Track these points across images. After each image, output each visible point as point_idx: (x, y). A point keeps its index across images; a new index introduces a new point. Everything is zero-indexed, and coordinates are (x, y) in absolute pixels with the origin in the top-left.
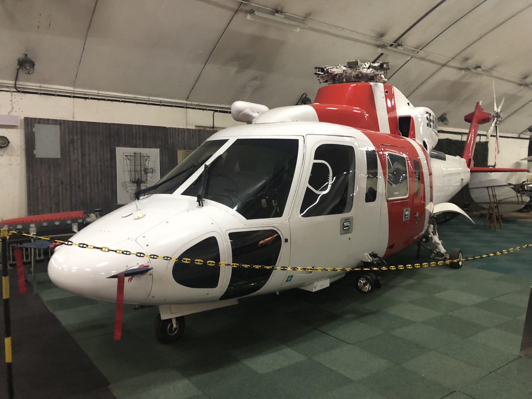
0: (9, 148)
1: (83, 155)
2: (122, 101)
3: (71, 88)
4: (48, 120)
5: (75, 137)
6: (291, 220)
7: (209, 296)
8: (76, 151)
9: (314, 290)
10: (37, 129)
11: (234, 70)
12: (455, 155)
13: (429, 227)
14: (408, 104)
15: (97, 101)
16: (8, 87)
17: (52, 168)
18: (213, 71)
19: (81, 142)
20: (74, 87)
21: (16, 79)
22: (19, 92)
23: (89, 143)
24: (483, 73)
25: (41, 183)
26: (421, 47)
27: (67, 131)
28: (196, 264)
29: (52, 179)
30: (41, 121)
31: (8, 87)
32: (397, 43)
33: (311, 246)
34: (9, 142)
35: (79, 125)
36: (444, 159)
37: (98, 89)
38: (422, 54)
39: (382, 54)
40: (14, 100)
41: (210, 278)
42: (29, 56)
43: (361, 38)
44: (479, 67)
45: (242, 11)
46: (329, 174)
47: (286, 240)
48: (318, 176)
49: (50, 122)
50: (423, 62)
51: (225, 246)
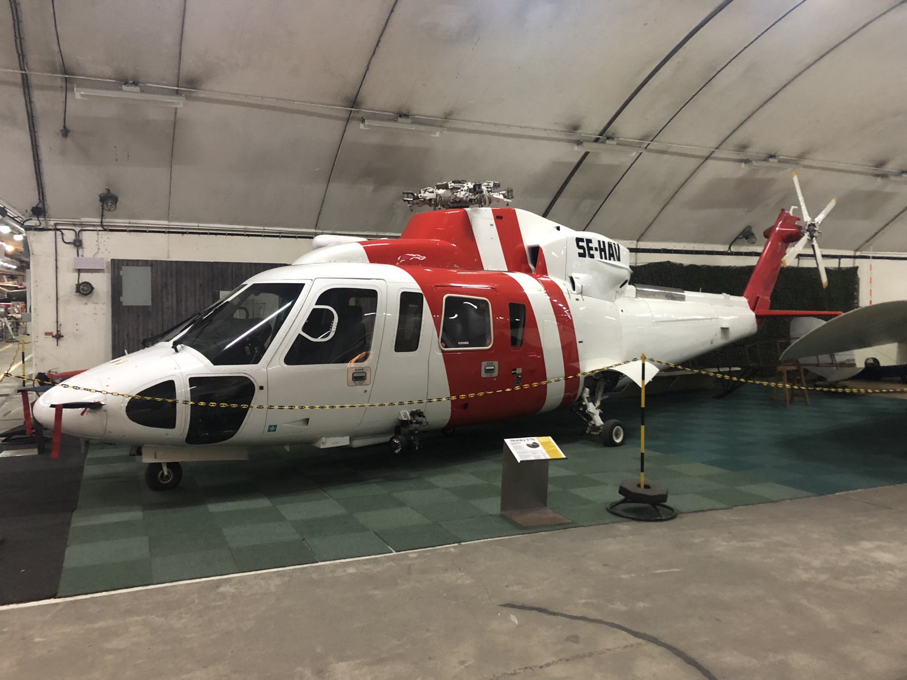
0: (94, 297)
1: (178, 302)
2: (229, 234)
3: (165, 223)
4: (138, 261)
6: (270, 367)
8: (170, 296)
9: (322, 447)
10: (125, 271)
11: (370, 188)
12: (720, 293)
13: (583, 389)
14: (558, 228)
16: (94, 226)
17: (141, 318)
18: (338, 190)
19: (177, 286)
20: (169, 220)
21: (102, 216)
22: (105, 230)
24: (781, 165)
25: (128, 336)
26: (649, 138)
28: (153, 404)
29: (141, 330)
30: (129, 263)
31: (94, 226)
32: (605, 135)
33: (286, 393)
34: (93, 288)
36: (682, 298)
37: (198, 222)
38: (654, 146)
39: (587, 154)
41: (169, 421)
42: (112, 191)
43: (544, 134)
44: (772, 156)
45: (354, 119)
47: (261, 388)
49: (140, 263)
50: (666, 157)
51: (183, 391)
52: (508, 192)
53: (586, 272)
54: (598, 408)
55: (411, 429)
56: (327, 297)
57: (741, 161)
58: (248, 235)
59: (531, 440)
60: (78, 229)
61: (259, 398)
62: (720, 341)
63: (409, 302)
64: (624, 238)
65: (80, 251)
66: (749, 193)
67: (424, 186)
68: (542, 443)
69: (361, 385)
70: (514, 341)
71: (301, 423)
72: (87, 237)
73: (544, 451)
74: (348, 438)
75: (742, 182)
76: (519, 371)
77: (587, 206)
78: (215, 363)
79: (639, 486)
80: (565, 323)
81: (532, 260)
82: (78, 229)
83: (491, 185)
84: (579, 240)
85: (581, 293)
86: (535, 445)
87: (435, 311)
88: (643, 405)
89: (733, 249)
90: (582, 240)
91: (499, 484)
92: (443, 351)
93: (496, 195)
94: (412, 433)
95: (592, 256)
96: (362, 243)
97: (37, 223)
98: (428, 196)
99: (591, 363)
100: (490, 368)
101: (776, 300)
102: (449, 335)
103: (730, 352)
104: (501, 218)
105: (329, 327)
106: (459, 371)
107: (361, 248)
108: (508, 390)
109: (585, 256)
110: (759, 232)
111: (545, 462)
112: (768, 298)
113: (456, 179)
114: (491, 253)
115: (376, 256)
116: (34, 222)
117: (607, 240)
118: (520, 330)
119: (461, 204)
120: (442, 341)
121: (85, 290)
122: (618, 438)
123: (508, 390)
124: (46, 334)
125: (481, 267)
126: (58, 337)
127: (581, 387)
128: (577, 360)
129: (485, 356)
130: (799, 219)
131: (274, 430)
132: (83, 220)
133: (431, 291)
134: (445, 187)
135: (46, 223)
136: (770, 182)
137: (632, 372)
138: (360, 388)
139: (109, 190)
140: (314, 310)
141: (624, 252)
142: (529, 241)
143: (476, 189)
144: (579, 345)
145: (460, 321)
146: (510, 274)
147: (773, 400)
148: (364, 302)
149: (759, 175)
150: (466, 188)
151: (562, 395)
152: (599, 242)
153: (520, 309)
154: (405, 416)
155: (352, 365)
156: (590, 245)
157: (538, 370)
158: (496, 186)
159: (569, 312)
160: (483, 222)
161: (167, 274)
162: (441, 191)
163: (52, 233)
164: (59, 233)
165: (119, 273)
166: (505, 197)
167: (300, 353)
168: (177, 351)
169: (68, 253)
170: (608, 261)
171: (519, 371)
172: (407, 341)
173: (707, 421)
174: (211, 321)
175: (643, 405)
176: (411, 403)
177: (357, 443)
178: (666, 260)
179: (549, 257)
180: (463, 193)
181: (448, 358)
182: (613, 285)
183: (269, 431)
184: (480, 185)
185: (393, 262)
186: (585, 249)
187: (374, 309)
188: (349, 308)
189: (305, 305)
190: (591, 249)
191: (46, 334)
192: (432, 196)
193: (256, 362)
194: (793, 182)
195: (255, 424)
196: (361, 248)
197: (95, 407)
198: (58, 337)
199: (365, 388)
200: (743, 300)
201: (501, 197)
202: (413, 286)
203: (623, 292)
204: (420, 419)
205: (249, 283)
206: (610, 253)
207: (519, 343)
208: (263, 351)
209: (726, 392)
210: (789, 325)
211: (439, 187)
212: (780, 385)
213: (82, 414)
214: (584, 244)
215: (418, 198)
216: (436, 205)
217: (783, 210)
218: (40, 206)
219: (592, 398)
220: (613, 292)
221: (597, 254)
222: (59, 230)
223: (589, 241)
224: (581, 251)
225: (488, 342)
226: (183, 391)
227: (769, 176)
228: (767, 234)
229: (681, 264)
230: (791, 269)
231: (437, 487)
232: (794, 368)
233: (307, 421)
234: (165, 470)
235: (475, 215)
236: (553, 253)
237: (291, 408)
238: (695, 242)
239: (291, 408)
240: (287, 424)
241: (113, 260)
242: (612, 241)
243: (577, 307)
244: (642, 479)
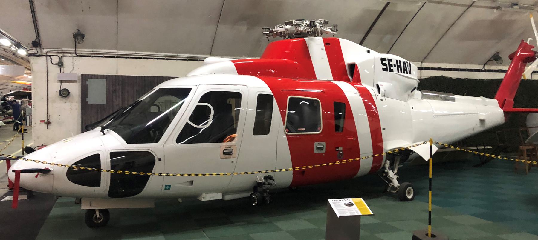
0: (70, 98)
2: (155, 59)
3: (115, 51)
5: (117, 88)
6: (166, 145)
7: (95, 192)
8: (117, 98)
9: (203, 200)
10: (90, 82)
11: (244, 28)
13: (386, 161)
14: (369, 52)
15: (135, 59)
16: (70, 53)
20: (117, 50)
21: (75, 47)
22: (78, 56)
23: (128, 92)
24: (522, 10)
27: (111, 83)
28: (85, 170)
31: (70, 53)
34: (69, 93)
35: (121, 79)
36: (454, 100)
40: (75, 62)
41: (96, 183)
42: (81, 31)
44: (515, 4)
46: (210, 113)
47: (160, 159)
48: (199, 114)
50: (441, 5)
51: (105, 162)
52: (334, 27)
53: (388, 82)
54: (396, 174)
55: (264, 188)
56: (207, 97)
57: (494, 8)
58: (168, 59)
59: (347, 201)
60: (60, 55)
61: (157, 168)
62: (479, 129)
63: (264, 101)
64: (414, 61)
65: (62, 69)
66: (498, 29)
67: (277, 24)
68: (356, 203)
69: (230, 158)
70: (337, 127)
71: (188, 184)
72: (66, 60)
73: (357, 209)
74: (221, 194)
75: (493, 23)
76: (341, 149)
77: (388, 38)
78: (128, 142)
79: (427, 235)
80: (373, 116)
81: (351, 73)
82: (60, 55)
83: (322, 22)
84: (383, 59)
85: (384, 96)
86: (350, 205)
87: (282, 107)
88: (430, 176)
89: (487, 68)
90: (385, 59)
91: (325, 229)
92: (287, 135)
93: (325, 29)
94: (264, 191)
95: (392, 71)
96: (233, 61)
97: (36, 51)
98: (279, 30)
99: (392, 143)
100: (320, 147)
101: (517, 102)
102: (291, 124)
103: (486, 136)
104: (329, 44)
105: (207, 118)
106: (299, 149)
107: (232, 65)
108: (331, 164)
109: (387, 71)
110: (505, 57)
111: (359, 216)
112: (512, 100)
113: (298, 19)
114: (322, 69)
115: (242, 69)
116: (34, 51)
117: (402, 60)
118: (342, 120)
119: (301, 35)
120: (287, 127)
121: (64, 94)
122: (409, 195)
123: (331, 164)
124: (41, 121)
125: (315, 78)
126: (48, 123)
127: (384, 159)
128: (381, 141)
129: (318, 138)
130: (533, 47)
131: (169, 189)
132: (64, 49)
133: (279, 93)
134: (291, 23)
135: (41, 52)
136: (511, 23)
137: (424, 151)
138: (228, 160)
139: (79, 30)
140: (198, 106)
141: (414, 66)
142: (348, 60)
143: (312, 24)
144: (383, 132)
145: (299, 116)
146: (336, 83)
147: (517, 170)
148: (233, 101)
149: (507, 17)
150: (305, 24)
151: (371, 165)
152: (397, 61)
153: (341, 106)
154: (260, 179)
155: (224, 145)
156: (391, 63)
157: (354, 149)
158: (326, 23)
159: (376, 108)
160: (317, 48)
161: (117, 84)
162: (288, 27)
163: (45, 58)
164: (49, 58)
165: (86, 83)
166: (332, 30)
167: (187, 134)
168: (104, 134)
169: (54, 70)
170: (403, 74)
171: (341, 149)
172: (262, 127)
173: (470, 183)
174: (130, 113)
175: (430, 176)
176: (267, 172)
177: (228, 197)
178: (440, 75)
179: (363, 71)
180: (303, 27)
181: (290, 139)
182: (407, 90)
183: (165, 189)
184: (314, 22)
185: (254, 74)
186: (387, 66)
187: (239, 106)
188: (221, 105)
189: (190, 103)
190: (391, 65)
191: (41, 121)
192: (282, 30)
193: (157, 141)
194: (530, 22)
195: (154, 185)
196: (233, 64)
197: (46, 171)
198: (48, 123)
199: (232, 160)
200: (495, 101)
201: (329, 30)
202: (267, 91)
203: (413, 95)
204: (271, 181)
205: (157, 88)
206: (403, 68)
207: (340, 129)
208: (162, 134)
209: (483, 163)
210: (526, 118)
211: (286, 24)
212: (523, 161)
213: (36, 176)
214: (386, 62)
215: (272, 31)
216: (285, 37)
217: (523, 41)
218: (37, 41)
219: (392, 168)
220: (406, 96)
221: (395, 69)
222: (49, 56)
223: (390, 60)
224: (385, 67)
225: (319, 129)
226: (105, 162)
227: (513, 18)
228: (511, 57)
229: (451, 78)
230: (527, 81)
231: (283, 230)
232: (531, 147)
233: (192, 182)
234: (98, 214)
235: (311, 42)
236: (366, 71)
237: (175, 175)
238: (460, 63)
239: (175, 175)
240: (179, 186)
241: (82, 75)
242: (406, 61)
243: (382, 105)
244: (430, 229)
